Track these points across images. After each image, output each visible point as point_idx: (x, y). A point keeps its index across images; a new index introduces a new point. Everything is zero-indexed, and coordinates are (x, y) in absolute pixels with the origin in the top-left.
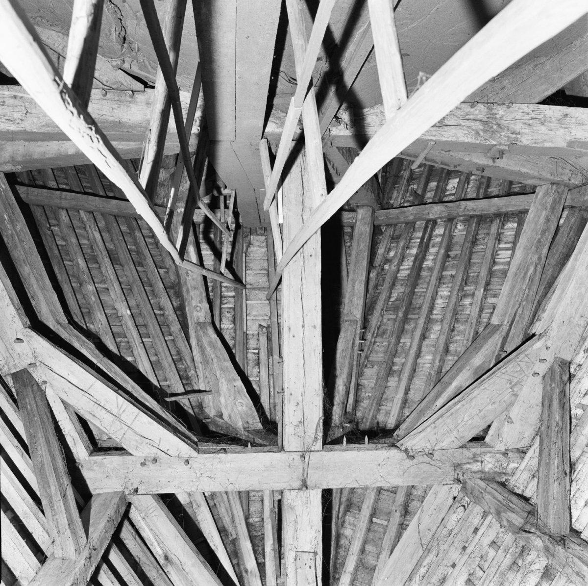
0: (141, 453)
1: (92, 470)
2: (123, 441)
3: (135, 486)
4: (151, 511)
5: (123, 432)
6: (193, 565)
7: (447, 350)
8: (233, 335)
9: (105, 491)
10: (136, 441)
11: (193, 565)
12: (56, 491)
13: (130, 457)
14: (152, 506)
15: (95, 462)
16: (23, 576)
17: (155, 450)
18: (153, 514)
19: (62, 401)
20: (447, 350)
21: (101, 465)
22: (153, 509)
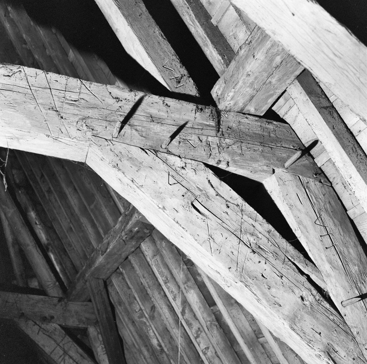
0: (53, 325)
1: (86, 318)
2: (64, 336)
3: (60, 304)
4: (52, 285)
5: (63, 342)
6: (28, 245)
7: (338, 325)
8: (168, 320)
9: (80, 303)
10: (55, 335)
11: (28, 245)
12: (123, 272)
13: (60, 323)
14: (50, 288)
15: (84, 323)
16: (119, 275)
17: (43, 326)
18: (50, 283)
19: (270, 333)
20: (338, 325)
21: (80, 321)
22: (50, 286)
